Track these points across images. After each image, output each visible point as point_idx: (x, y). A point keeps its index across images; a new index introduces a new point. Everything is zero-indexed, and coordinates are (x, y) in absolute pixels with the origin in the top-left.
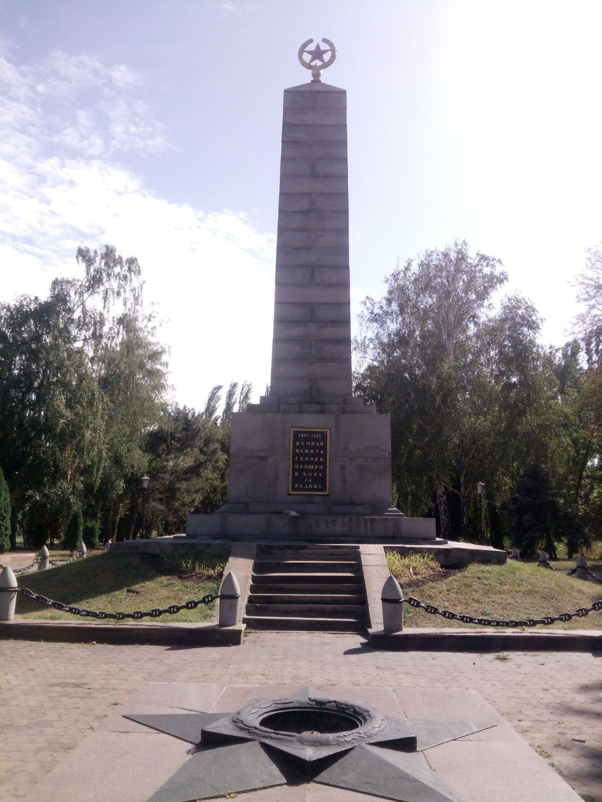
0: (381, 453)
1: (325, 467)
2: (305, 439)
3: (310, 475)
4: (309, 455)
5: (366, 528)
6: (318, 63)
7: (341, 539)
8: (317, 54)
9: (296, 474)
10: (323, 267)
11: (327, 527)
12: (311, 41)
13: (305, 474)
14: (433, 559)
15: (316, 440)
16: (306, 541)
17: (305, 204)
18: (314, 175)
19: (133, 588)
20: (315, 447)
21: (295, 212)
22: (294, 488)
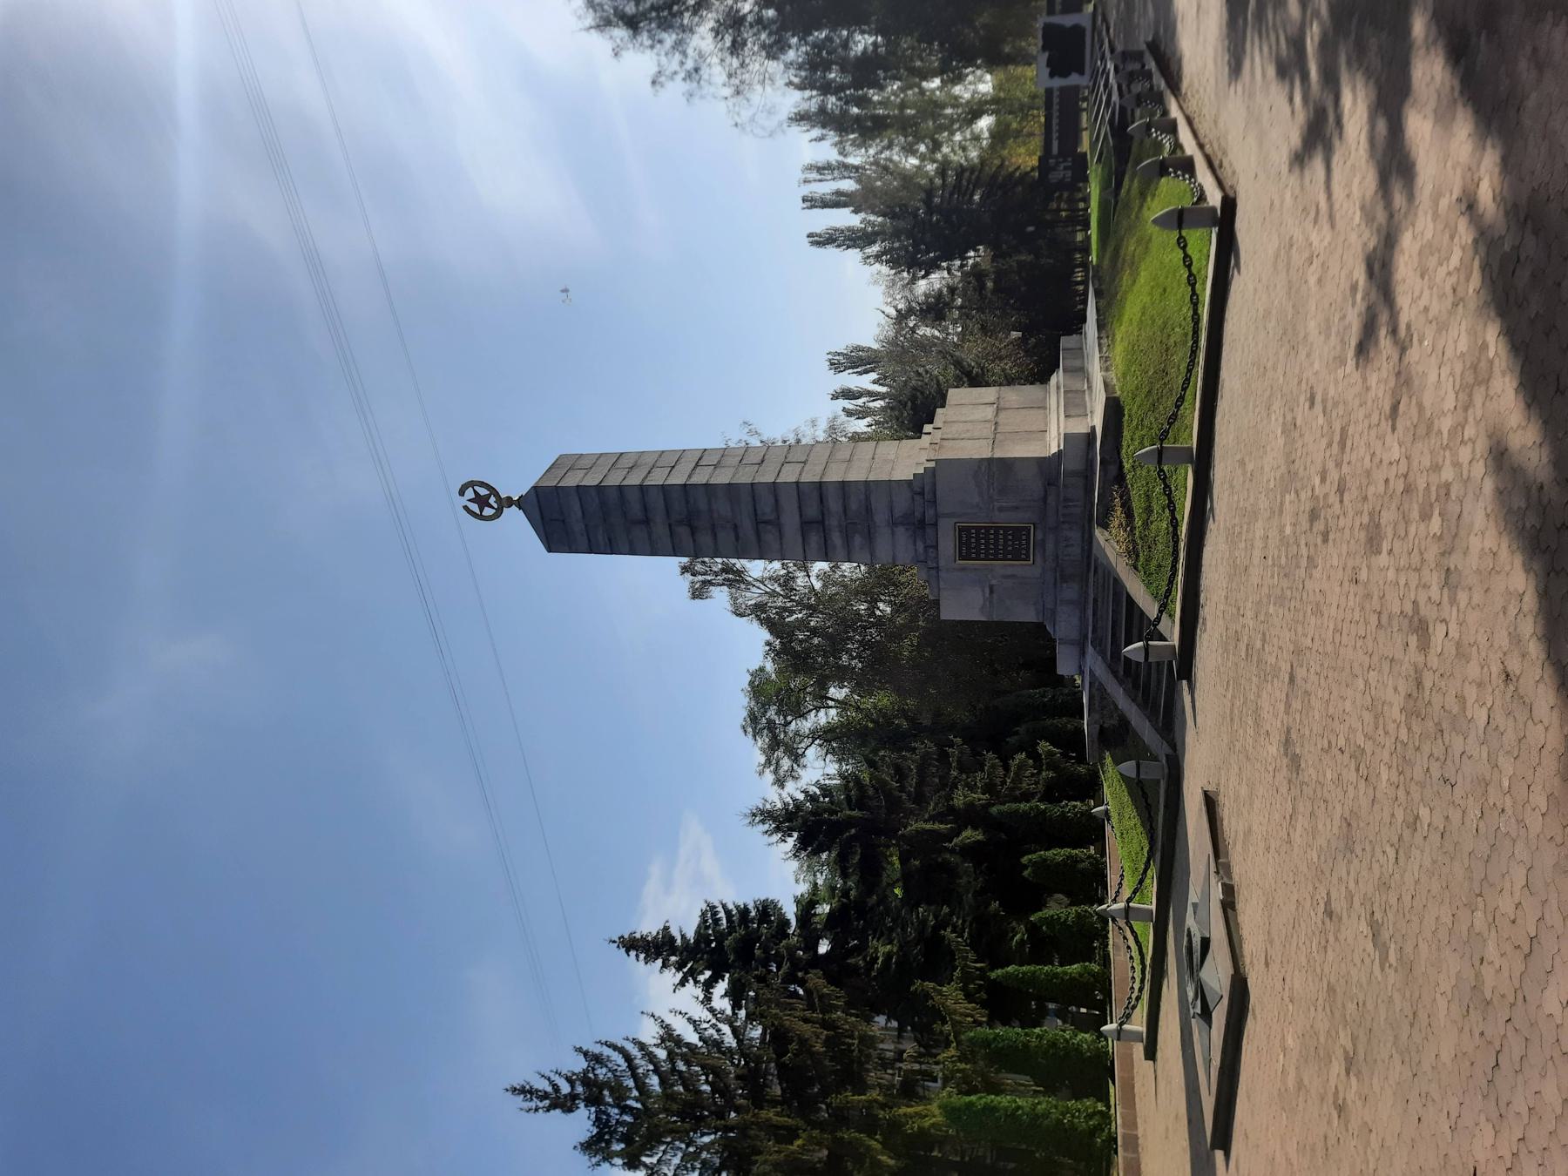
0: (983, 468)
1: (1001, 528)
2: (969, 548)
5: (1075, 506)
6: (492, 500)
7: (1110, 250)
8: (482, 501)
9: (1010, 556)
10: (755, 510)
11: (1072, 545)
12: (466, 508)
13: (1010, 548)
14: (1053, 916)
15: (969, 538)
16: (1089, 565)
17: (683, 531)
18: (647, 521)
19: (1480, 243)
20: (978, 539)
21: (694, 541)
22: (1027, 559)
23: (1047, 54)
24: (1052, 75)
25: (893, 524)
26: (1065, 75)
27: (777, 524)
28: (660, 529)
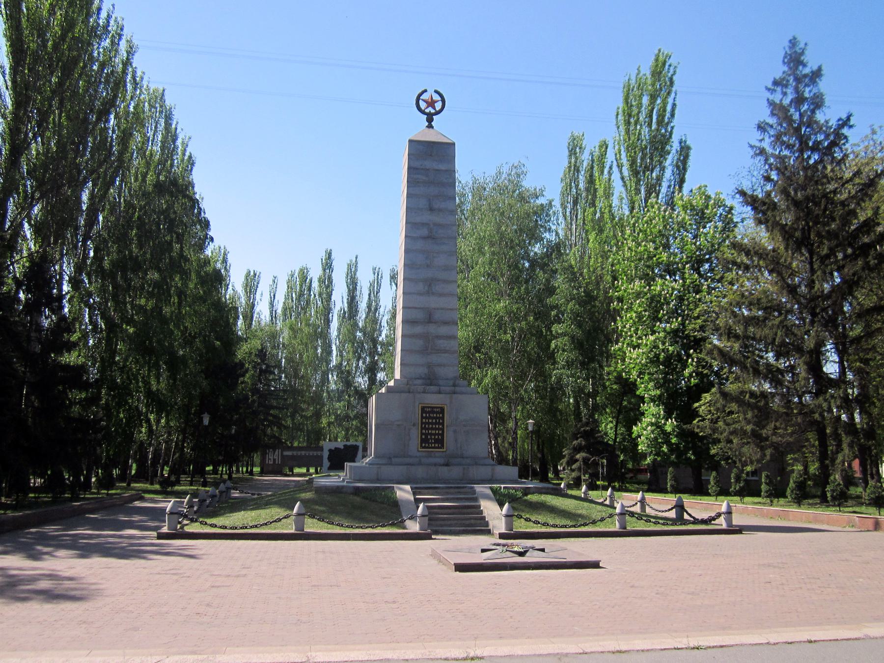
2: (429, 412)
3: (433, 437)
4: (432, 423)
9: (423, 437)
12: (425, 91)
13: (429, 437)
17: (424, 232)
20: (436, 418)
23: (342, 447)
24: (330, 451)
25: (429, 366)
26: (329, 459)
27: (429, 293)
28: (426, 217)
